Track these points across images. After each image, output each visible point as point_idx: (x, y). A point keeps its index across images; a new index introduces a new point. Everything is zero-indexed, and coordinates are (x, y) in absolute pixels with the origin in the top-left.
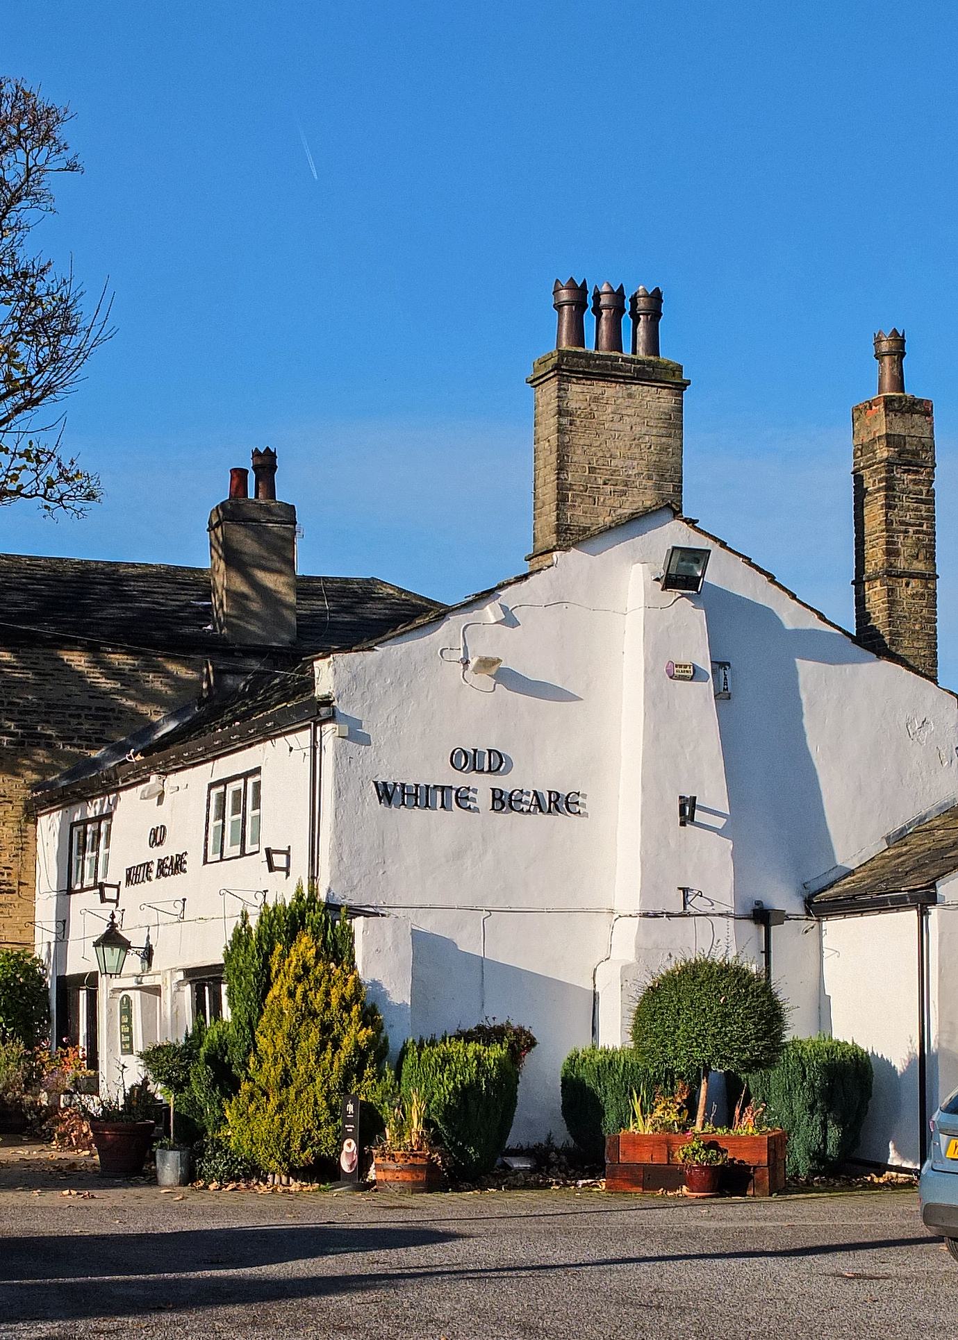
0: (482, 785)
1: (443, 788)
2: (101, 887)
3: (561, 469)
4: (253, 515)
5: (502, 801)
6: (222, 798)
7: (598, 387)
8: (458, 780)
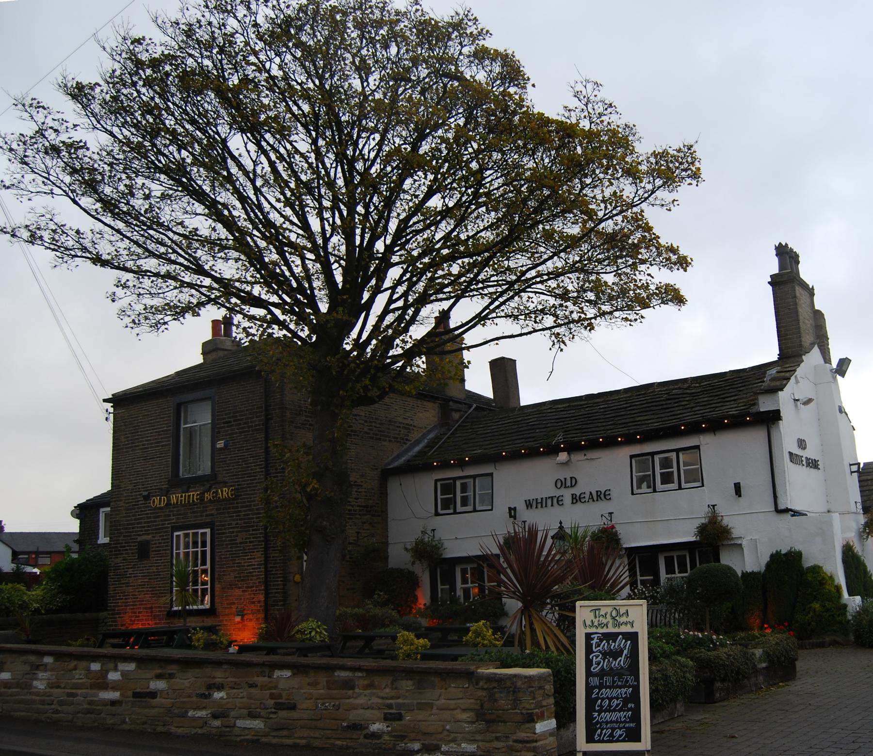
0: (567, 494)
1: (552, 498)
8: (558, 493)
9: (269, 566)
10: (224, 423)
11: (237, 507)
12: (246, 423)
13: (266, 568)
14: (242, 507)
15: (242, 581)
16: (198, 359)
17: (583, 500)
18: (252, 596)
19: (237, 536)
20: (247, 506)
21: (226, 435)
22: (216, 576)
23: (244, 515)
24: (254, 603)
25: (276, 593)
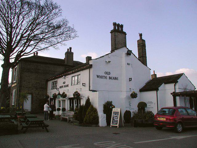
0: (108, 76)
2: (57, 88)
3: (115, 41)
4: (69, 54)
5: (110, 78)
6: (53, 83)
7: (119, 33)
8: (106, 75)
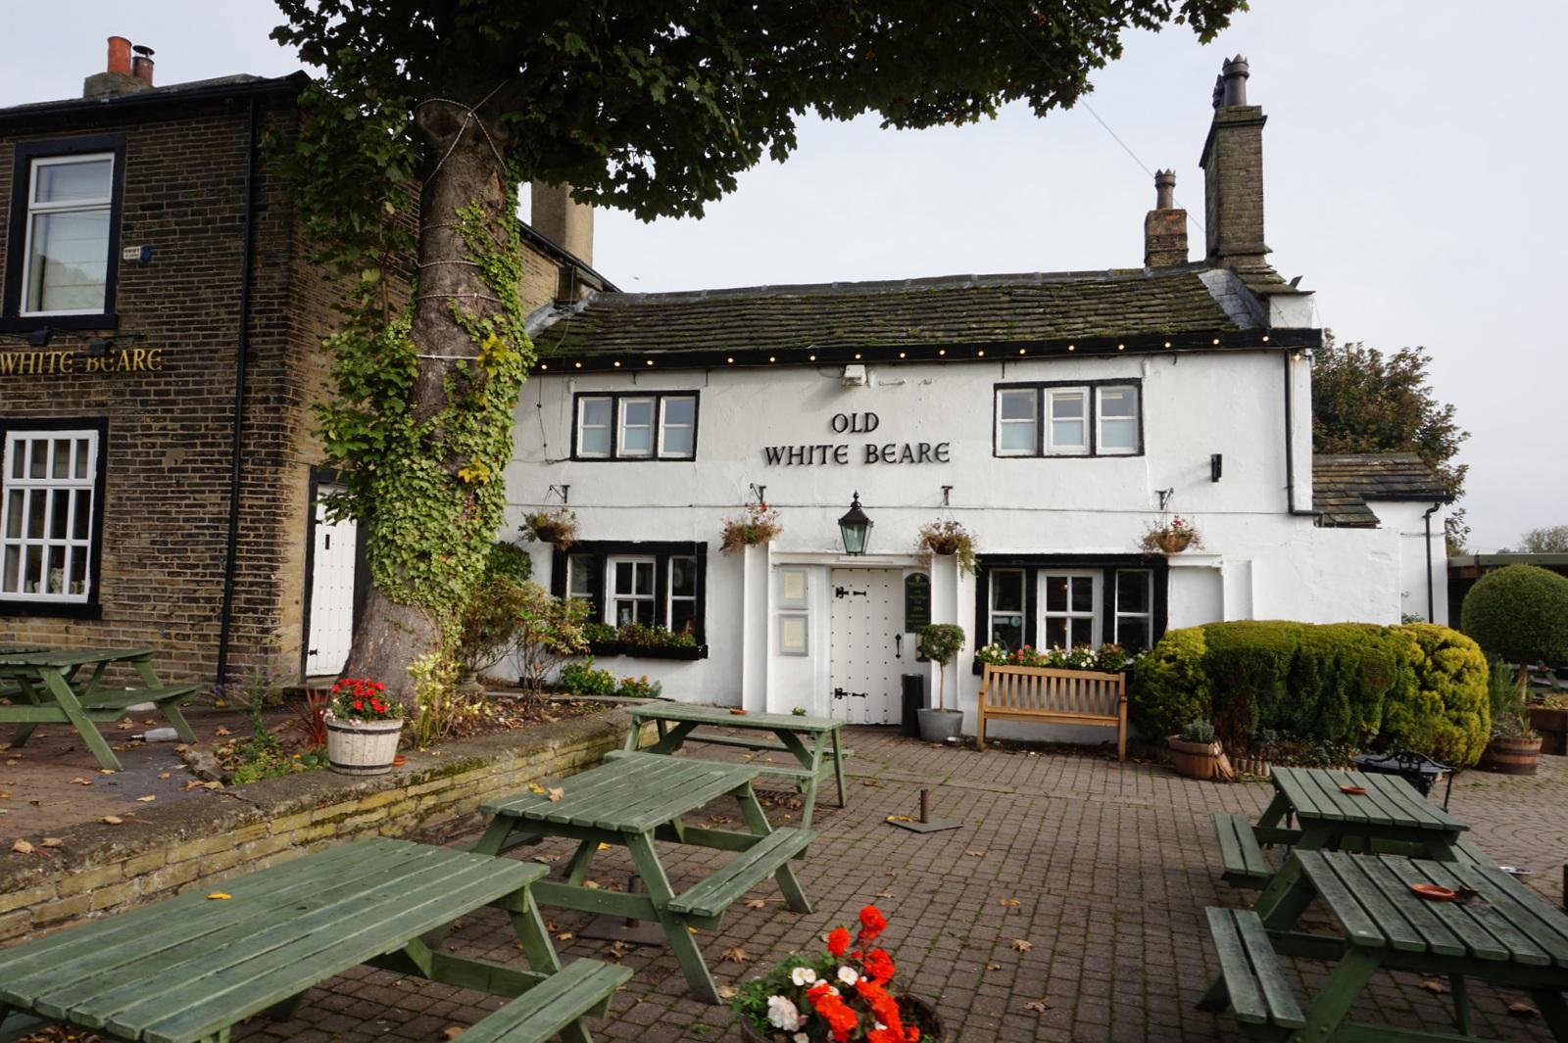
0: (856, 444)
8: (837, 440)
9: (241, 524)
10: (143, 208)
11: (167, 392)
12: (199, 213)
13: (233, 528)
14: (177, 393)
15: (172, 551)
16: (76, 92)
17: (889, 459)
18: (193, 586)
19: (163, 454)
20: (190, 392)
21: (147, 235)
22: (106, 535)
23: (183, 411)
24: (196, 600)
25: (252, 584)
